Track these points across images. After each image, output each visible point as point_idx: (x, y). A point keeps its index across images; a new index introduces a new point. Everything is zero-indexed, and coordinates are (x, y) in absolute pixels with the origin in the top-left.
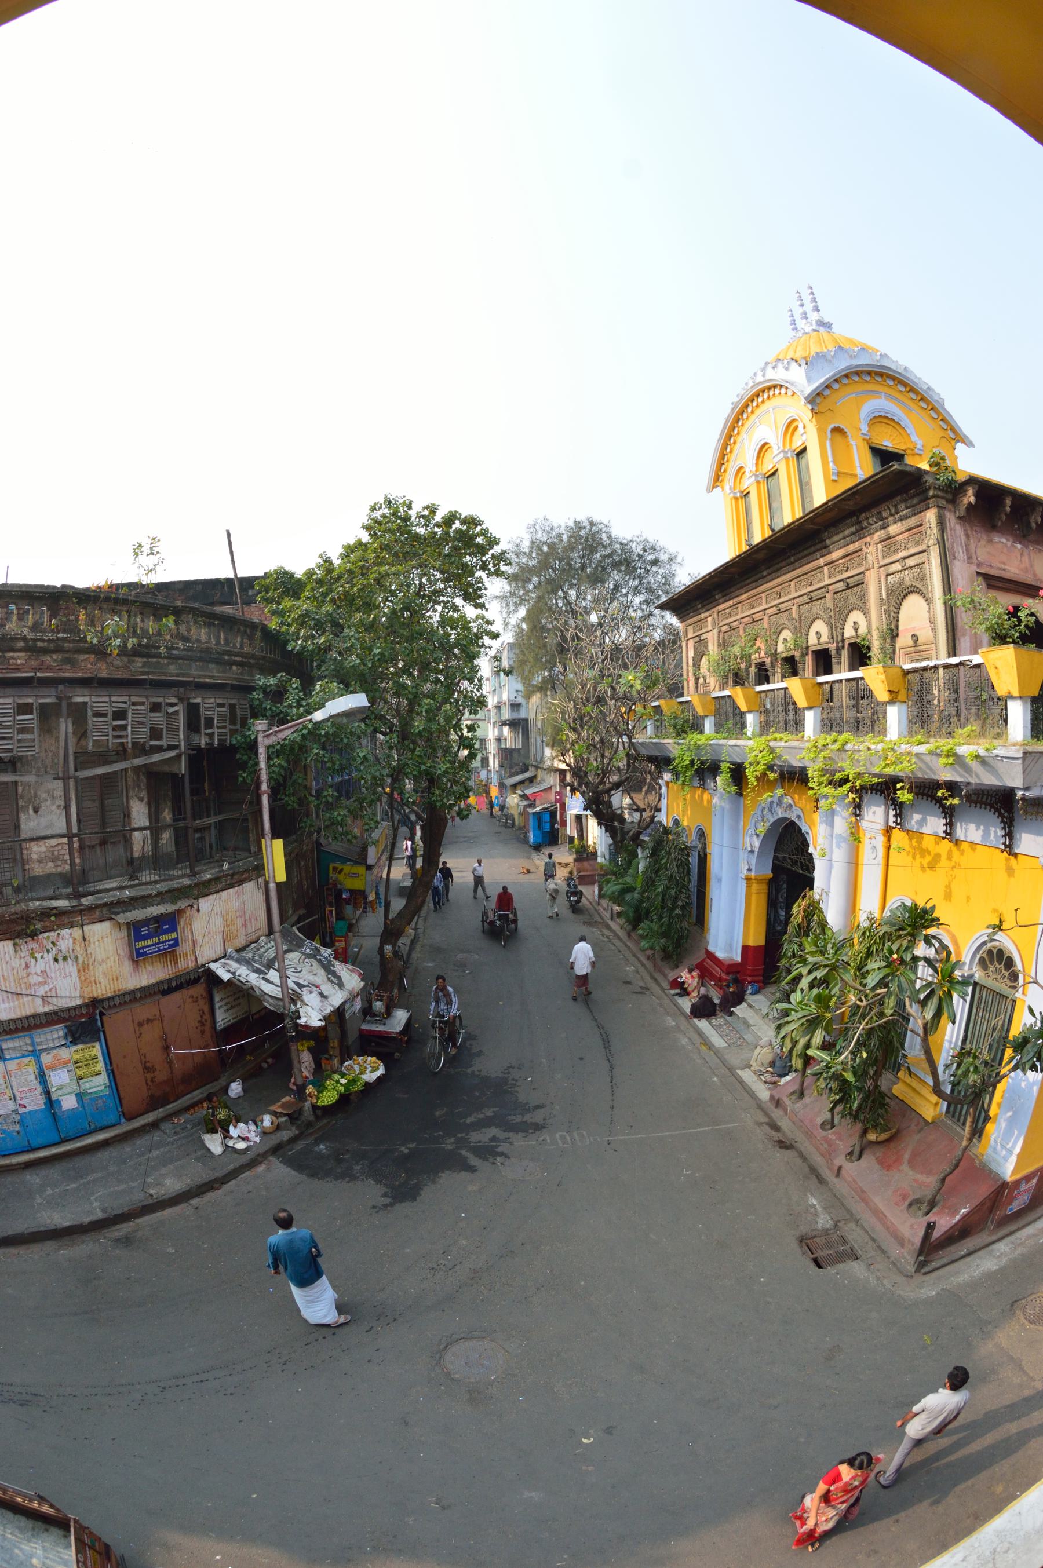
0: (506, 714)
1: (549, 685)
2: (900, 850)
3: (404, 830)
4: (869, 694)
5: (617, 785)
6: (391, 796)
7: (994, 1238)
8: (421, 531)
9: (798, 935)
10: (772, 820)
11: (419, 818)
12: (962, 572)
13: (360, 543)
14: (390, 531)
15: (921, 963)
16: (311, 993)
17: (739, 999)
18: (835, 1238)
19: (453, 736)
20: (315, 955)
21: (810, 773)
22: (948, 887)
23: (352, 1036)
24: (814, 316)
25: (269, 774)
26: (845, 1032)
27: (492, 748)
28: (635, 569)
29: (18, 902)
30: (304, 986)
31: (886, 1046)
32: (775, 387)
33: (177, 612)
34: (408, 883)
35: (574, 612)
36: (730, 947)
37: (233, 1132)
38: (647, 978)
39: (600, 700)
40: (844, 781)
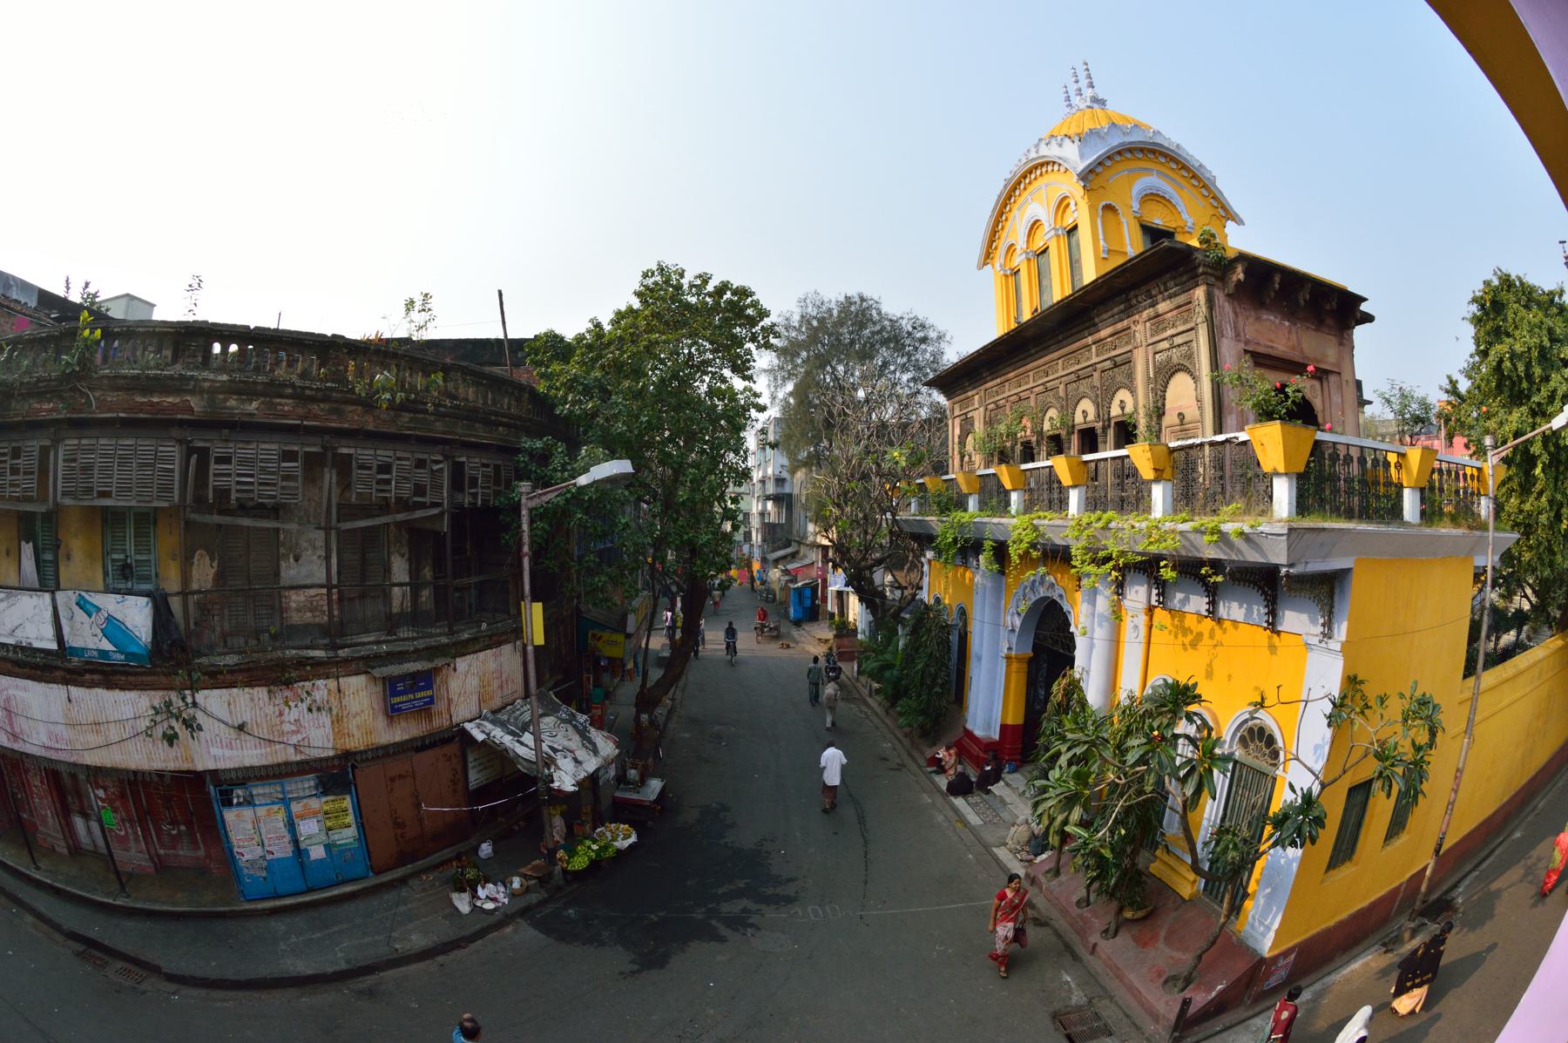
0: (771, 489)
1: (815, 461)
2: (1162, 628)
3: (664, 601)
4: (1134, 472)
5: (879, 562)
6: (652, 566)
7: (1251, 1013)
8: (693, 300)
9: (1058, 713)
11: (680, 589)
12: (1229, 349)
13: (630, 310)
14: (663, 299)
15: (1181, 741)
17: (996, 777)
18: (1089, 1014)
19: (717, 508)
20: (571, 720)
21: (1073, 551)
22: (1210, 665)
23: (605, 803)
24: (1088, 93)
25: (531, 537)
26: (1103, 811)
27: (755, 522)
28: (904, 346)
29: (274, 649)
31: (1144, 822)
32: (1048, 163)
33: (446, 370)
34: (666, 654)
35: (842, 388)
36: (988, 726)
37: (481, 893)
38: (905, 756)
39: (865, 477)
40: (1108, 559)
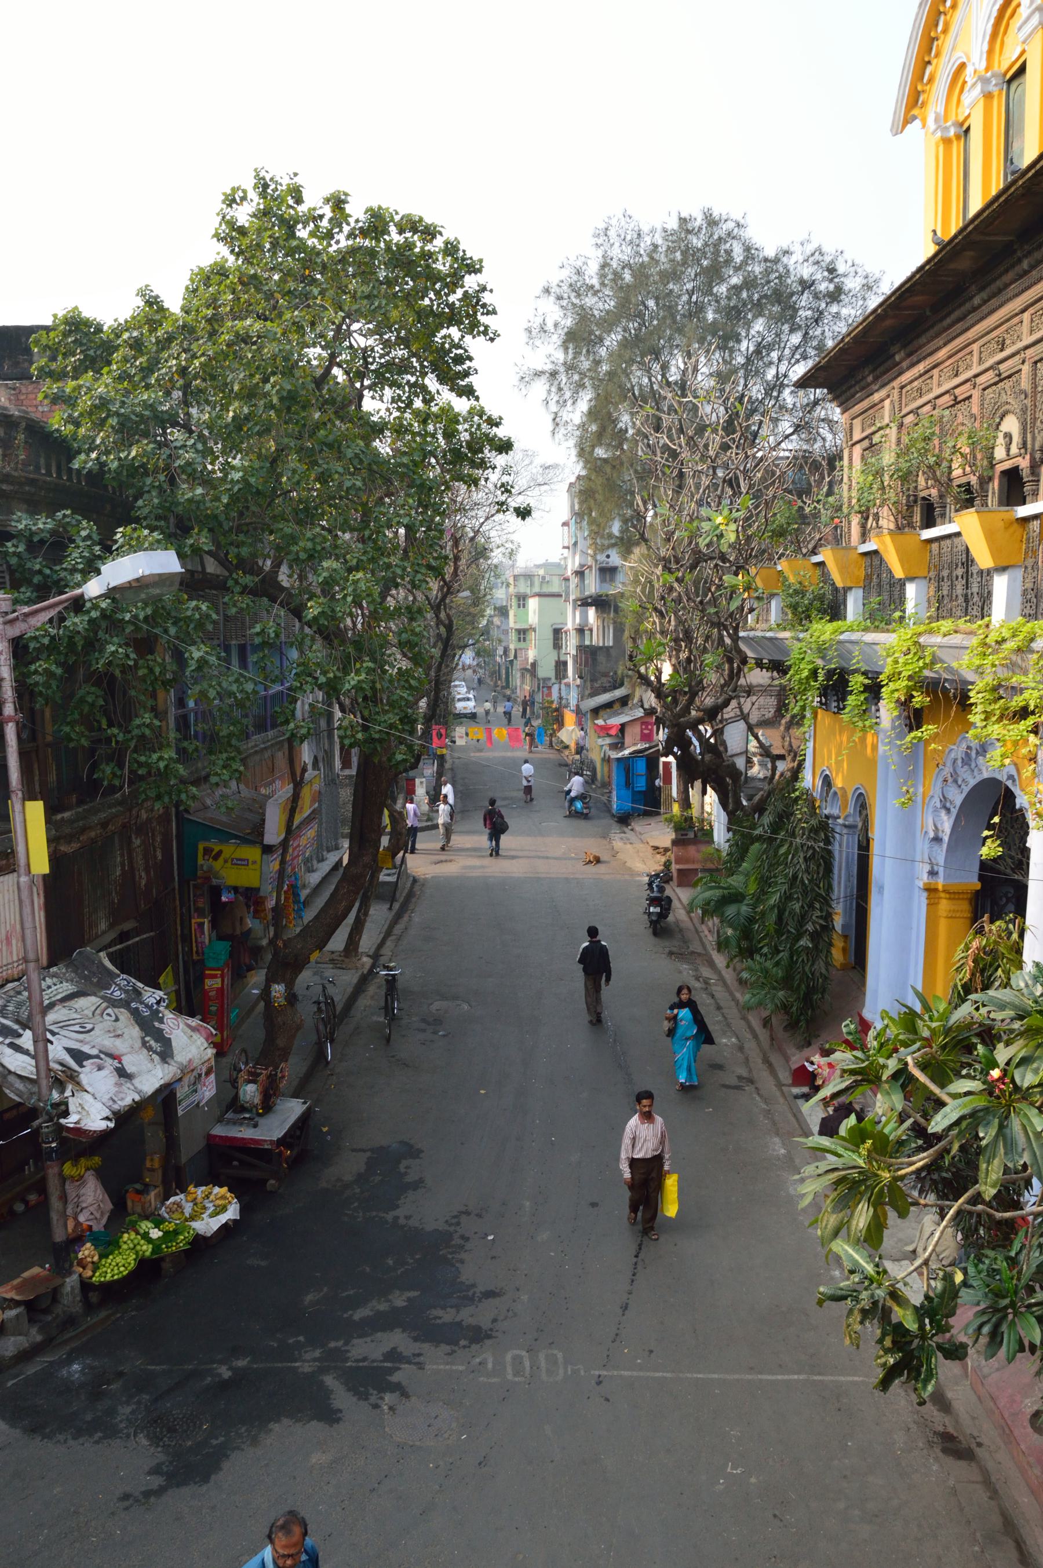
10: (972, 782)
13: (220, 271)
16: (100, 1068)
20: (129, 1002)
23: (189, 1147)
30: (89, 1057)
